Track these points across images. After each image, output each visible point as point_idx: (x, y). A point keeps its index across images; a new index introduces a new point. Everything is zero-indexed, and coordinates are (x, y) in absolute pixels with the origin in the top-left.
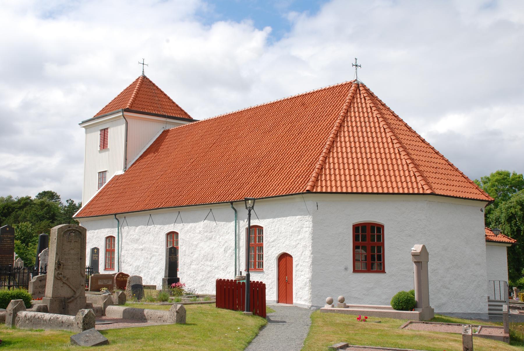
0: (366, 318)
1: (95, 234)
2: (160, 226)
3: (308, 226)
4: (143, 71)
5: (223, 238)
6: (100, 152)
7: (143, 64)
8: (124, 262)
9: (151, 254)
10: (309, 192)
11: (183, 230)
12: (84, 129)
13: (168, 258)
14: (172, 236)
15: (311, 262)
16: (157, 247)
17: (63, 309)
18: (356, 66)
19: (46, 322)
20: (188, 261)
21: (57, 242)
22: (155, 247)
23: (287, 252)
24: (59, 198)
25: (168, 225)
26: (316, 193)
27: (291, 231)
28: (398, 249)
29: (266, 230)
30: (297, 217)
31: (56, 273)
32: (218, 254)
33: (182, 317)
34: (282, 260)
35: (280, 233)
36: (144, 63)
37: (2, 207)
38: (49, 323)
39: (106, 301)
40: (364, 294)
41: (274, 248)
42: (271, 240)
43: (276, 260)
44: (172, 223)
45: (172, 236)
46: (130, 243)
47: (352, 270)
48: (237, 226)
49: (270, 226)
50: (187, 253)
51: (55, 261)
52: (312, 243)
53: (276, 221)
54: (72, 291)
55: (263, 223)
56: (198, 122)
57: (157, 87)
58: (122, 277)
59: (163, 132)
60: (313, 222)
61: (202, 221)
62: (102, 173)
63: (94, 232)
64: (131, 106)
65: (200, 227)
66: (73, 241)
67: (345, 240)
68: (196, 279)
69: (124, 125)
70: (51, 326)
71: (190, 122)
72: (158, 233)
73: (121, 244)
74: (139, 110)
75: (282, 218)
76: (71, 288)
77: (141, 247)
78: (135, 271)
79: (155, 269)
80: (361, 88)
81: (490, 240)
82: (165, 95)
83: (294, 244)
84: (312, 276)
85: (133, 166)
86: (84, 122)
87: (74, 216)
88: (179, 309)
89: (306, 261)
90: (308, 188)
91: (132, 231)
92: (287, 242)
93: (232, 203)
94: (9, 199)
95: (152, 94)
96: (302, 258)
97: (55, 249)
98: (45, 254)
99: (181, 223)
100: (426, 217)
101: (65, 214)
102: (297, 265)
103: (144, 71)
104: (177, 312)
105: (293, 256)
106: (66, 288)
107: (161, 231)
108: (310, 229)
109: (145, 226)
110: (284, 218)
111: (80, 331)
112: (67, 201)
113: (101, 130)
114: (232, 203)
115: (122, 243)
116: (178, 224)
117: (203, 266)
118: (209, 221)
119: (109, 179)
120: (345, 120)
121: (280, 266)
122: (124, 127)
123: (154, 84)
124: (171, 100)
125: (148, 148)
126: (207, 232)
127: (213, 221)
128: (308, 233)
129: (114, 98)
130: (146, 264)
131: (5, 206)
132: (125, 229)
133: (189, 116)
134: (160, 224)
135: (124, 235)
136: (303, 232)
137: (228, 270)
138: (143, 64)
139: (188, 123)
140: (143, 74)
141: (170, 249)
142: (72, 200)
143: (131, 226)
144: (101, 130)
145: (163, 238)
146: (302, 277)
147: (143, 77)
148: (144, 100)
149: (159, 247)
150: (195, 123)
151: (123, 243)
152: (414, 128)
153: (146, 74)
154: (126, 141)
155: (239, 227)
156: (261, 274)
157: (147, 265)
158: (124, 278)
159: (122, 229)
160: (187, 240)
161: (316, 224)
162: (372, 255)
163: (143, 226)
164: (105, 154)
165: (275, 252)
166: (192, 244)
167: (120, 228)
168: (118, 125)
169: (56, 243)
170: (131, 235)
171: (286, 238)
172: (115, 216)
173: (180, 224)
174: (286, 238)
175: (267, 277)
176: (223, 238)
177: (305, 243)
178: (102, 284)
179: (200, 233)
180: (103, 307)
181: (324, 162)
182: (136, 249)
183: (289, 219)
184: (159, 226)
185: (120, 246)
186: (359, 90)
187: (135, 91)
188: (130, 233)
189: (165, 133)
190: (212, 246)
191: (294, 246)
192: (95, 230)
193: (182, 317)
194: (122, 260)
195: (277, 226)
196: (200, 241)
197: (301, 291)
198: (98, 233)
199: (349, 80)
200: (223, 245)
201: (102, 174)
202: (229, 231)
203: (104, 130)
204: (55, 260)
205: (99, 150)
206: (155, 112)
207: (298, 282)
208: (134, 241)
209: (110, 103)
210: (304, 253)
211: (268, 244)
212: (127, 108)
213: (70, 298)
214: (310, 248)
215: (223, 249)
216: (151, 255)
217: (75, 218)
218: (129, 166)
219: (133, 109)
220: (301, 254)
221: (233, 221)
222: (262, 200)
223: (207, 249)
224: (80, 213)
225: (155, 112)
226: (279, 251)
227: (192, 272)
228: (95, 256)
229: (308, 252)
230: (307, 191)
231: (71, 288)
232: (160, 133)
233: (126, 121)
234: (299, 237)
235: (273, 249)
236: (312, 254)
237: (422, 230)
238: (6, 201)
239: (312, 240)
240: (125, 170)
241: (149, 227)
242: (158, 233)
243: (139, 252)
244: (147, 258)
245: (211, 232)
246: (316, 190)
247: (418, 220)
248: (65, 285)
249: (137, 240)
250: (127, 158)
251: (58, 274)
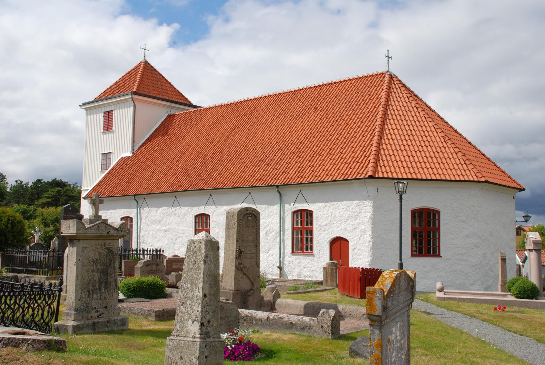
1: (109, 214)
2: (188, 208)
3: (368, 210)
5: (264, 221)
6: (103, 133)
7: (145, 49)
8: (143, 243)
9: (176, 235)
10: (371, 177)
11: (216, 213)
12: (84, 111)
15: (371, 246)
16: (183, 228)
17: (244, 303)
18: (389, 57)
19: (262, 322)
21: (237, 227)
22: (181, 228)
23: (342, 236)
24: (5, 178)
25: (197, 207)
26: (378, 178)
27: (347, 216)
29: (317, 214)
30: (355, 202)
31: (237, 262)
34: (336, 243)
35: (334, 217)
38: (267, 323)
39: (274, 294)
40: (421, 278)
41: (326, 232)
44: (203, 205)
46: (151, 224)
47: (410, 254)
48: (282, 209)
49: (322, 210)
51: (236, 249)
54: (251, 283)
55: (313, 207)
59: (167, 116)
61: (239, 204)
66: (251, 227)
69: (132, 107)
70: (270, 326)
71: (193, 108)
72: (185, 215)
73: (140, 225)
74: (145, 93)
75: (336, 203)
76: (250, 279)
77: (164, 228)
80: (395, 79)
82: (167, 80)
83: (351, 228)
85: (142, 148)
86: (84, 104)
89: (365, 245)
90: (370, 173)
91: (153, 212)
92: (342, 226)
95: (154, 79)
96: (360, 242)
97: (235, 236)
101: (14, 194)
102: (354, 249)
106: (246, 279)
107: (189, 213)
108: (370, 214)
109: (169, 207)
110: (339, 203)
111: (328, 336)
112: (16, 181)
113: (105, 113)
114: (277, 186)
116: (209, 207)
119: (114, 161)
121: (333, 250)
122: (132, 109)
124: (172, 86)
127: (253, 204)
128: (368, 218)
129: (115, 82)
130: (170, 245)
132: (145, 211)
133: (190, 102)
135: (144, 216)
136: (362, 216)
137: (270, 252)
138: (145, 49)
142: (21, 180)
145: (191, 220)
148: (149, 84)
149: (186, 229)
150: (199, 109)
151: (142, 224)
152: (446, 119)
154: (134, 123)
155: (284, 210)
156: (311, 257)
157: (171, 246)
159: (142, 210)
160: (221, 222)
162: (428, 240)
163: (167, 208)
165: (328, 236)
167: (139, 209)
168: (125, 107)
169: (236, 229)
170: (152, 216)
171: (341, 222)
172: (134, 197)
173: (212, 207)
174: (341, 222)
176: (264, 221)
177: (363, 228)
178: (176, 267)
180: (272, 299)
182: (158, 230)
184: (186, 208)
185: (139, 227)
186: (393, 81)
187: (139, 75)
189: (170, 118)
191: (350, 230)
194: (141, 241)
195: (330, 211)
198: (111, 213)
199: (380, 71)
201: (106, 156)
202: (272, 214)
203: (109, 112)
204: (235, 248)
205: (102, 131)
208: (156, 222)
209: (111, 86)
210: (362, 238)
211: (319, 228)
213: (249, 291)
214: (370, 233)
216: (177, 237)
218: (136, 148)
219: (140, 92)
221: (277, 204)
222: (314, 184)
226: (332, 235)
229: (368, 236)
231: (250, 279)
233: (134, 104)
234: (357, 221)
236: (372, 238)
239: (372, 224)
241: (174, 209)
242: (185, 215)
244: (172, 239)
248: (245, 277)
251: (239, 264)
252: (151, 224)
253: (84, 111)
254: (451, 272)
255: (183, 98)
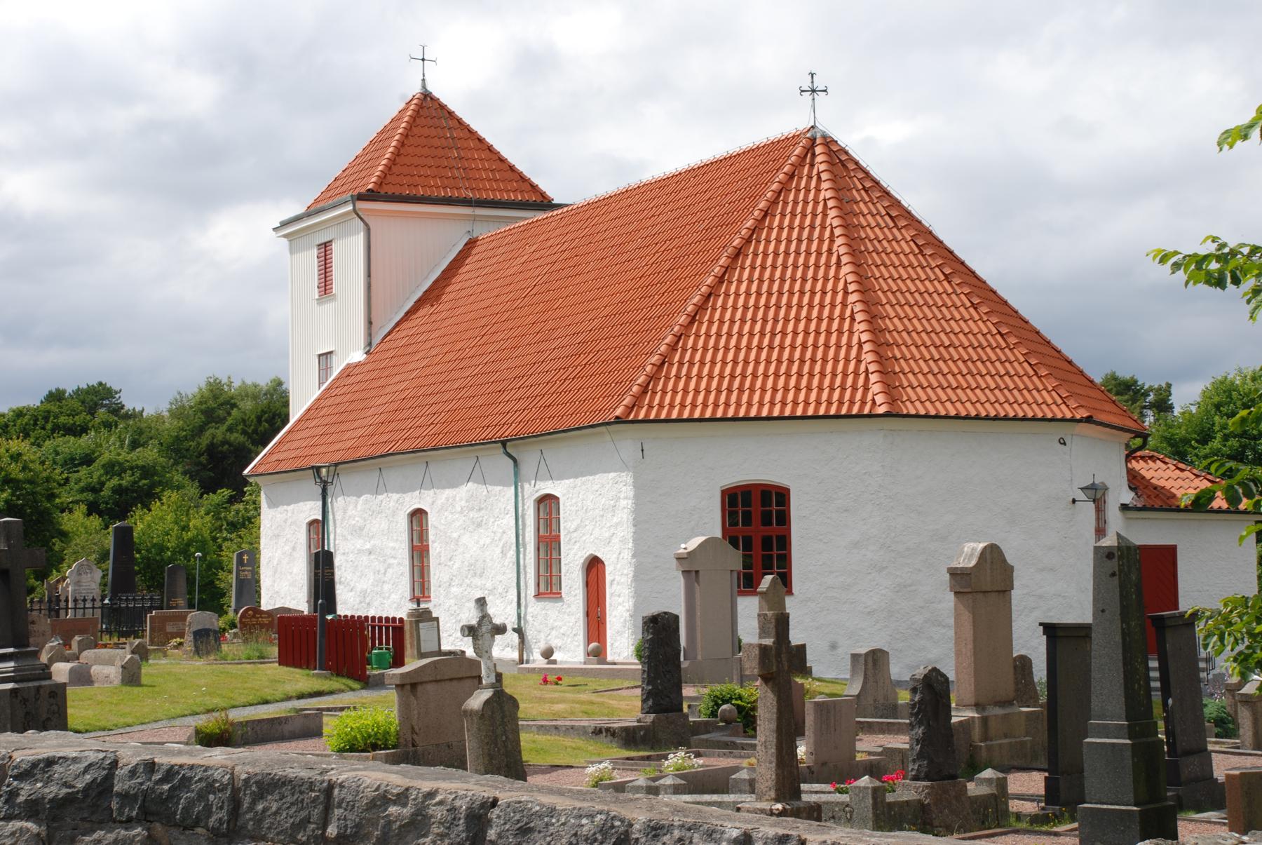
0: (559, 679)
1: (289, 514)
2: (398, 496)
4: (424, 80)
6: (320, 301)
7: (423, 60)
8: (340, 583)
10: (619, 421)
13: (313, 574)
14: (418, 516)
15: (631, 575)
18: (813, 91)
20: (445, 578)
22: (392, 544)
28: (821, 540)
32: (491, 560)
33: (133, 675)
35: (586, 510)
36: (421, 61)
37: (253, 417)
41: (578, 544)
42: (573, 526)
43: (580, 573)
45: (418, 516)
46: (349, 537)
50: (443, 559)
52: (634, 533)
53: (579, 484)
56: (565, 209)
57: (460, 121)
58: (254, 616)
60: (634, 487)
62: (325, 357)
63: (287, 511)
64: (382, 181)
65: (461, 500)
67: (705, 523)
68: (459, 618)
69: (362, 233)
73: (335, 540)
77: (368, 546)
78: (361, 602)
79: (393, 596)
81: (1174, 507)
82: (481, 140)
84: (635, 605)
86: (284, 224)
87: (245, 472)
88: (127, 662)
93: (504, 443)
94: (275, 390)
96: (619, 566)
98: (78, 571)
99: (430, 490)
100: (882, 466)
103: (426, 77)
104: (122, 667)
105: (606, 563)
108: (630, 502)
110: (591, 478)
115: (335, 536)
117: (469, 590)
118: (476, 485)
120: (754, 237)
122: (360, 238)
123: (451, 114)
125: (426, 291)
126: (472, 509)
131: (262, 411)
134: (397, 493)
138: (423, 60)
139: (541, 215)
140: (424, 87)
141: (317, 554)
143: (348, 496)
144: (319, 245)
146: (620, 607)
147: (423, 97)
150: (560, 211)
153: (430, 88)
157: (379, 588)
158: (258, 618)
161: (641, 490)
164: (329, 307)
165: (580, 554)
166: (450, 537)
175: (569, 610)
179: (461, 512)
181: (673, 348)
182: (360, 551)
183: (599, 479)
184: (395, 496)
188: (349, 513)
189: (471, 244)
190: (482, 542)
192: (289, 504)
193: (133, 675)
196: (462, 531)
197: (618, 638)
200: (500, 540)
205: (317, 297)
206: (446, 192)
207: (614, 620)
209: (343, 171)
212: (369, 190)
214: (631, 545)
215: (498, 550)
217: (247, 476)
218: (377, 340)
219: (390, 190)
220: (618, 558)
223: (475, 549)
224: (260, 464)
225: (446, 192)
227: (452, 601)
228: (244, 571)
229: (627, 555)
230: (617, 417)
232: (460, 247)
233: (366, 224)
235: (576, 547)
237: (874, 496)
238: (265, 394)
239: (635, 526)
240: (369, 351)
241: (380, 497)
243: (365, 558)
244: (379, 571)
245: (480, 509)
246: (637, 414)
247: (866, 473)
249: (361, 529)
250: (373, 321)
252: (349, 537)
253: (285, 240)
254: (817, 628)
255: (526, 186)
